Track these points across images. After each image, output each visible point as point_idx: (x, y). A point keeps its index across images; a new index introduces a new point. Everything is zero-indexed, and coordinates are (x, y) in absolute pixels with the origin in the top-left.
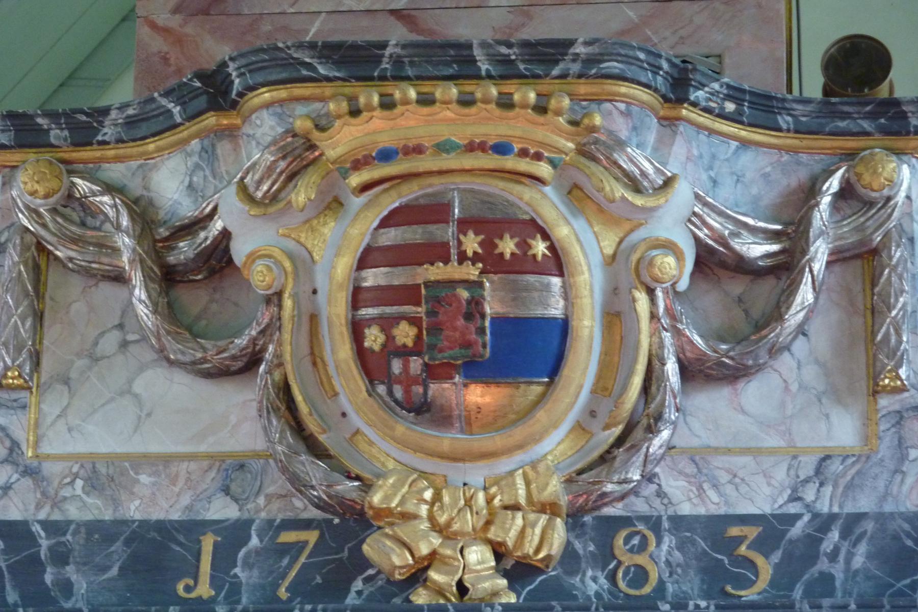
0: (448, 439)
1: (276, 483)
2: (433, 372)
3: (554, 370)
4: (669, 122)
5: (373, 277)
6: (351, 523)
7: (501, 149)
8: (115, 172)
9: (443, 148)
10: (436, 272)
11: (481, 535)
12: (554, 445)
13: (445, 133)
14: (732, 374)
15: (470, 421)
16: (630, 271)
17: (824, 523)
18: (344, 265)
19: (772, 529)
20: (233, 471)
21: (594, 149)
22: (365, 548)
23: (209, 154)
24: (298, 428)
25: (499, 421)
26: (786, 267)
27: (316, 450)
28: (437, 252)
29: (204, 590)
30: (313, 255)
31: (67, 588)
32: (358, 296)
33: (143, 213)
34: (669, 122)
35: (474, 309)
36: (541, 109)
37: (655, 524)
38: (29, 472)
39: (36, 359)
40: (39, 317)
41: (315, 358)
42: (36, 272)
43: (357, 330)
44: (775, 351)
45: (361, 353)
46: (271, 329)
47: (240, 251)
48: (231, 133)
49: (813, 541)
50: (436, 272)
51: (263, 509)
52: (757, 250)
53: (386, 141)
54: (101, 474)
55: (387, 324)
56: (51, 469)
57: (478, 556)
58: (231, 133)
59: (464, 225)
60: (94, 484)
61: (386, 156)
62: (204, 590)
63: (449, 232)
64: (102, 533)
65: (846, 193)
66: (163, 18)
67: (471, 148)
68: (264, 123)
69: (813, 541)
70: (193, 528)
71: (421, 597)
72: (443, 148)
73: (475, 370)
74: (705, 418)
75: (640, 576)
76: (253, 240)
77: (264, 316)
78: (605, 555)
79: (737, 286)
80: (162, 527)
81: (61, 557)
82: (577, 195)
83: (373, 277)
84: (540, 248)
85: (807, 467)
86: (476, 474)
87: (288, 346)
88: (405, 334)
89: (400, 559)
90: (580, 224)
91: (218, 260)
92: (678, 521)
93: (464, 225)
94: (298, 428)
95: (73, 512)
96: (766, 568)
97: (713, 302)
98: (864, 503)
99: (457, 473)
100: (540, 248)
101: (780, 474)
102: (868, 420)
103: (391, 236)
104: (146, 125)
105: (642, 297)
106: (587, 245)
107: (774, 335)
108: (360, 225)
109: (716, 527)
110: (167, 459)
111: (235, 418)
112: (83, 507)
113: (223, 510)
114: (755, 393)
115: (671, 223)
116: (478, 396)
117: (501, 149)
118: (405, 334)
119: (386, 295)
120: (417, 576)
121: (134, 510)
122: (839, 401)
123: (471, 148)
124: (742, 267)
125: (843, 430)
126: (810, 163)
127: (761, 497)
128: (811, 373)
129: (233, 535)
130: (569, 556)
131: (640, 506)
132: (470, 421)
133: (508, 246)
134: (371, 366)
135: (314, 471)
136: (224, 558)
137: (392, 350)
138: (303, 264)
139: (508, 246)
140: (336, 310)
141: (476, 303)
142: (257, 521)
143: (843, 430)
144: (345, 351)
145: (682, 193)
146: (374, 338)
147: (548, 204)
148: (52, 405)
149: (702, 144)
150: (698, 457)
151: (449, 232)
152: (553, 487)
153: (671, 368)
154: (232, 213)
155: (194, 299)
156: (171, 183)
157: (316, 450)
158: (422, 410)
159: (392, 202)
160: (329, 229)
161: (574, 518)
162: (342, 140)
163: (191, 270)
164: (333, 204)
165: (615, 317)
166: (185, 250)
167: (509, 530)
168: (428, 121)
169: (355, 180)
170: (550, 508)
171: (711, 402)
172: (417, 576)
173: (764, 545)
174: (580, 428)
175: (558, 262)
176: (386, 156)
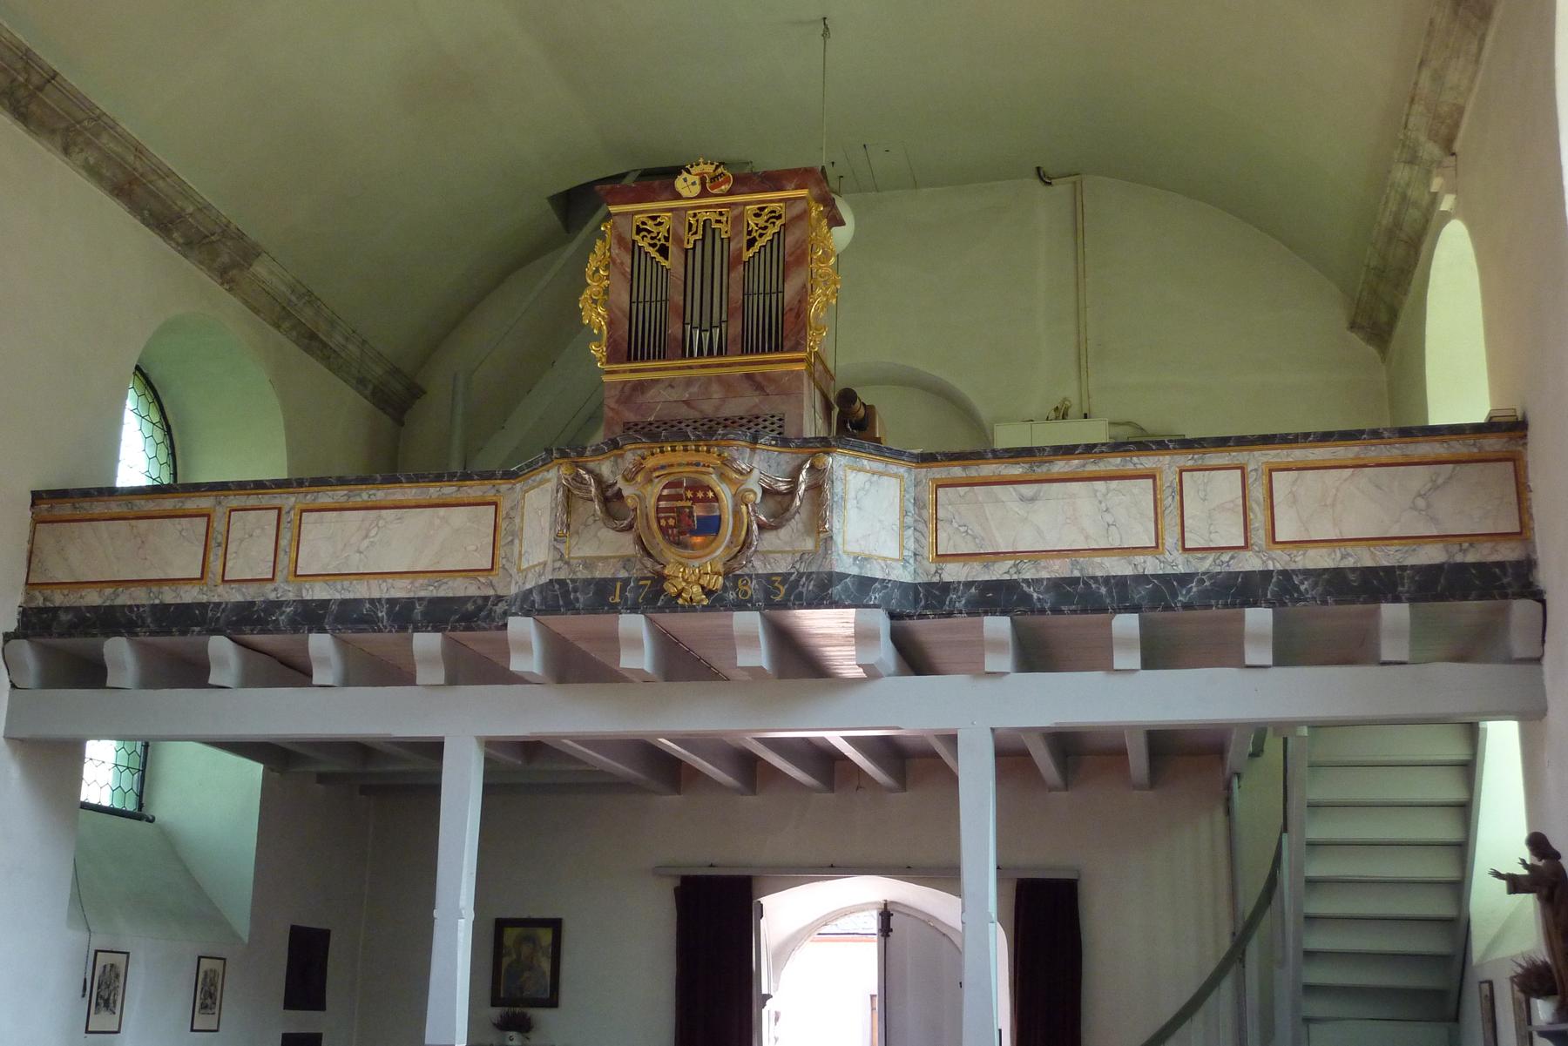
2: (683, 533)
3: (717, 531)
4: (753, 450)
5: (663, 504)
7: (697, 464)
8: (591, 465)
9: (680, 465)
10: (679, 504)
11: (697, 582)
12: (720, 551)
13: (679, 460)
14: (776, 528)
15: (693, 547)
16: (740, 499)
17: (801, 575)
18: (653, 501)
19: (785, 577)
20: (626, 562)
21: (726, 462)
25: (704, 546)
26: (792, 492)
27: (650, 555)
28: (679, 497)
29: (617, 600)
30: (645, 495)
31: (577, 600)
32: (658, 510)
33: (599, 479)
34: (753, 450)
36: (708, 451)
37: (750, 576)
38: (567, 563)
39: (568, 526)
41: (649, 527)
42: (568, 495)
43: (658, 520)
45: (660, 527)
46: (635, 519)
47: (625, 493)
48: (622, 456)
49: (797, 581)
50: (679, 504)
51: (635, 573)
52: (783, 487)
54: (588, 563)
55: (667, 518)
57: (696, 589)
58: (622, 456)
59: (687, 488)
60: (586, 567)
61: (663, 467)
62: (617, 600)
64: (588, 582)
65: (812, 466)
66: (613, 405)
67: (689, 464)
68: (630, 457)
69: (797, 581)
70: (614, 580)
72: (680, 465)
73: (695, 533)
74: (770, 540)
75: (745, 593)
77: (632, 514)
78: (735, 587)
79: (779, 498)
80: (605, 580)
81: (575, 591)
83: (663, 504)
84: (711, 494)
87: (639, 524)
88: (671, 522)
89: (673, 591)
90: (724, 486)
91: (619, 495)
92: (757, 575)
93: (687, 488)
95: (579, 575)
96: (783, 590)
97: (771, 504)
98: (814, 569)
100: (711, 494)
101: (789, 559)
102: (817, 542)
103: (665, 492)
104: (598, 451)
106: (725, 493)
107: (787, 515)
108: (657, 488)
109: (768, 577)
110: (607, 558)
111: (625, 544)
112: (583, 574)
113: (623, 574)
114: (782, 532)
115: (754, 485)
116: (698, 540)
117: (697, 464)
118: (671, 522)
120: (679, 595)
121: (597, 575)
123: (689, 464)
124: (778, 493)
125: (809, 544)
126: (803, 457)
127: (782, 568)
128: (800, 526)
129: (626, 582)
130: (725, 588)
132: (693, 547)
133: (700, 495)
135: (648, 562)
136: (623, 589)
138: (641, 498)
139: (700, 495)
140: (652, 514)
141: (691, 513)
142: (931, 475)
143: (809, 544)
144: (655, 526)
145: (756, 472)
146: (663, 523)
147: (713, 480)
148: (573, 542)
149: (764, 455)
153: (755, 527)
154: (621, 484)
156: (605, 469)
157: (650, 555)
158: (679, 544)
160: (649, 488)
162: (650, 463)
163: (611, 500)
164: (650, 481)
165: (736, 513)
166: (609, 493)
168: (677, 458)
170: (718, 573)
171: (769, 537)
172: (679, 595)
173: (783, 583)
174: (728, 547)
175: (716, 498)
176: (663, 467)
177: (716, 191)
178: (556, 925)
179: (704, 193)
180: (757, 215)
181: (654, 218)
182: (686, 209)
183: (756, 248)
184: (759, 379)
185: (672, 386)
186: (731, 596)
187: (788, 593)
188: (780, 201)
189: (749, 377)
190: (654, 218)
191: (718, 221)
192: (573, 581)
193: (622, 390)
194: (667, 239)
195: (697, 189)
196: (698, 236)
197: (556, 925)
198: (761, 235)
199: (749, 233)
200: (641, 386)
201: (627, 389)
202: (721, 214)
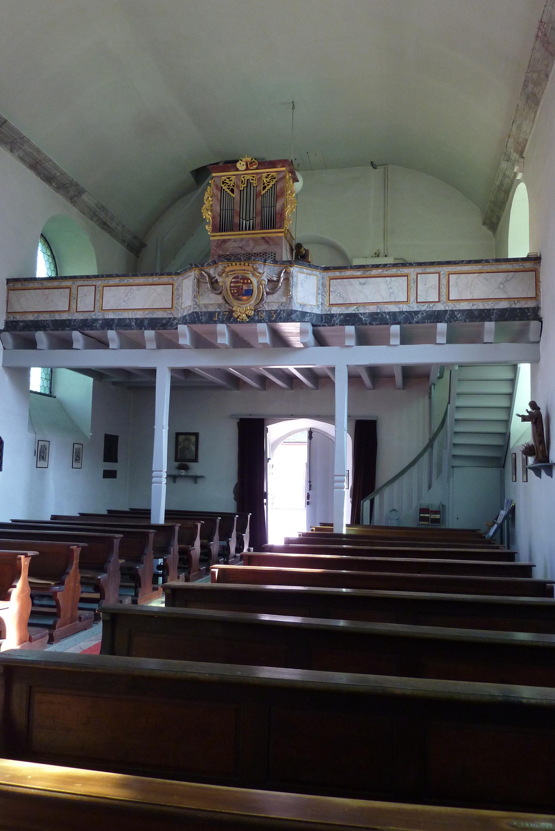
0: (241, 302)
1: (224, 307)
4: (265, 265)
5: (232, 285)
6: (231, 312)
7: (244, 270)
8: (206, 270)
10: (238, 284)
11: (244, 313)
13: (238, 268)
14: (272, 294)
16: (260, 283)
17: (281, 311)
19: (275, 311)
20: (219, 306)
21: (255, 269)
22: (92, 379)
23: (215, 269)
24: (226, 301)
26: (278, 281)
27: (228, 303)
28: (238, 282)
30: (226, 281)
31: (202, 319)
32: (231, 287)
34: (265, 265)
35: (242, 289)
36: (248, 265)
38: (198, 306)
39: (199, 292)
40: (199, 288)
42: (198, 282)
43: (231, 290)
44: (277, 291)
46: (222, 290)
47: (219, 281)
49: (280, 313)
50: (238, 284)
51: (223, 310)
52: (275, 279)
53: (232, 269)
54: (206, 306)
55: (233, 290)
56: (201, 305)
57: (244, 315)
58: (217, 267)
60: (205, 307)
61: (232, 271)
63: (239, 280)
64: (206, 313)
65: (285, 271)
66: (214, 248)
68: (220, 267)
69: (280, 313)
71: (238, 320)
73: (244, 295)
74: (271, 298)
75: (262, 317)
76: (220, 280)
77: (221, 288)
78: (258, 315)
79: (274, 283)
81: (201, 316)
82: (254, 275)
83: (232, 285)
84: (249, 281)
85: (280, 304)
86: (244, 306)
87: (224, 292)
88: (235, 291)
89: (236, 316)
90: (254, 278)
91: (217, 281)
94: (226, 301)
95: (203, 310)
97: (271, 285)
98: (286, 308)
99: (242, 306)
100: (249, 281)
102: (287, 298)
103: (233, 280)
104: (209, 265)
105: (261, 286)
106: (254, 281)
108: (230, 279)
109: (270, 311)
112: (204, 310)
113: (218, 310)
114: (275, 295)
115: (265, 278)
116: (245, 298)
117: (244, 270)
118: (235, 291)
119: (233, 287)
120: (238, 317)
121: (209, 310)
122: (284, 296)
124: (274, 281)
125: (284, 300)
127: (275, 308)
129: (219, 313)
130: (254, 315)
131: (262, 309)
132: (243, 300)
133: (246, 281)
134: (233, 294)
135: (227, 306)
136: (218, 316)
137: (234, 293)
139: (246, 281)
143: (284, 300)
144: (229, 293)
146: (232, 291)
147: (250, 276)
150: (268, 303)
151: (239, 280)
152: (252, 308)
153: (265, 293)
154: (217, 277)
155: (215, 285)
156: (212, 271)
157: (228, 303)
158: (238, 299)
159: (233, 276)
161: (255, 311)
162: (227, 269)
163: (214, 283)
164: (228, 276)
165: (258, 288)
167: (247, 313)
168: (237, 267)
169: (230, 274)
171: (270, 297)
173: (275, 313)
175: (251, 283)
176: (232, 271)
177: (251, 168)
178: (196, 435)
179: (247, 169)
180: (266, 177)
181: (229, 178)
182: (241, 175)
183: (266, 190)
184: (267, 239)
185: (235, 242)
186: (257, 318)
187: (277, 317)
188: (275, 172)
189: (263, 238)
190: (229, 178)
191: (252, 180)
192: (201, 312)
193: (217, 243)
194: (233, 186)
195: (245, 167)
196: (245, 185)
197: (196, 435)
198: (268, 185)
199: (264, 184)
200: (224, 241)
201: (219, 243)
202: (253, 177)
